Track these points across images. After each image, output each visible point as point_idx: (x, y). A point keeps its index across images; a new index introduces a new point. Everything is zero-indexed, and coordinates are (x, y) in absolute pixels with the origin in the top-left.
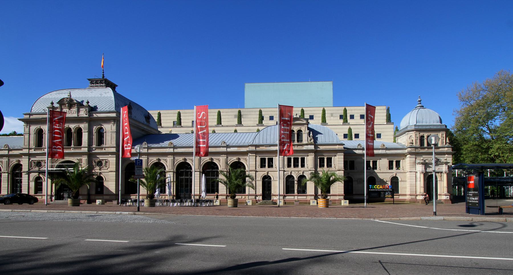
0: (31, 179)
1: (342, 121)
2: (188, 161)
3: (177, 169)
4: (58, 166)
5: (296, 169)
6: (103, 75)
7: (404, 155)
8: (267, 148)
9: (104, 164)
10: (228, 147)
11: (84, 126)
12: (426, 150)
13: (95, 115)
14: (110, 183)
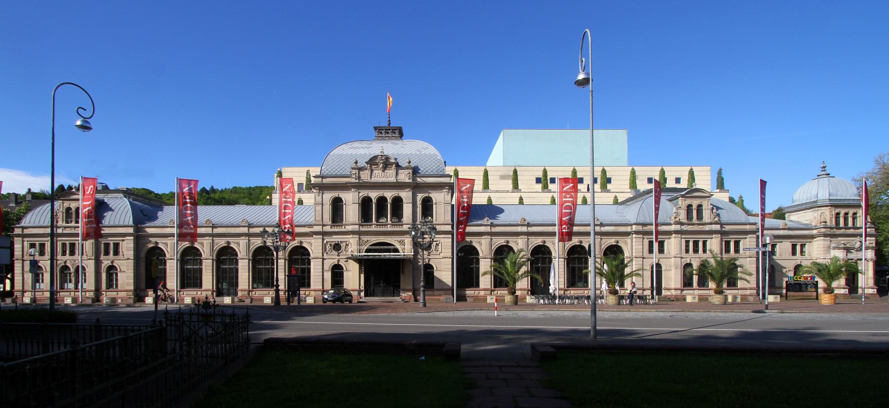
0: (327, 267)
1: (540, 186)
2: (304, 245)
3: (568, 254)
4: (368, 251)
5: (696, 255)
7: (813, 237)
9: (343, 248)
10: (528, 225)
12: (842, 231)
13: (419, 179)
14: (443, 273)
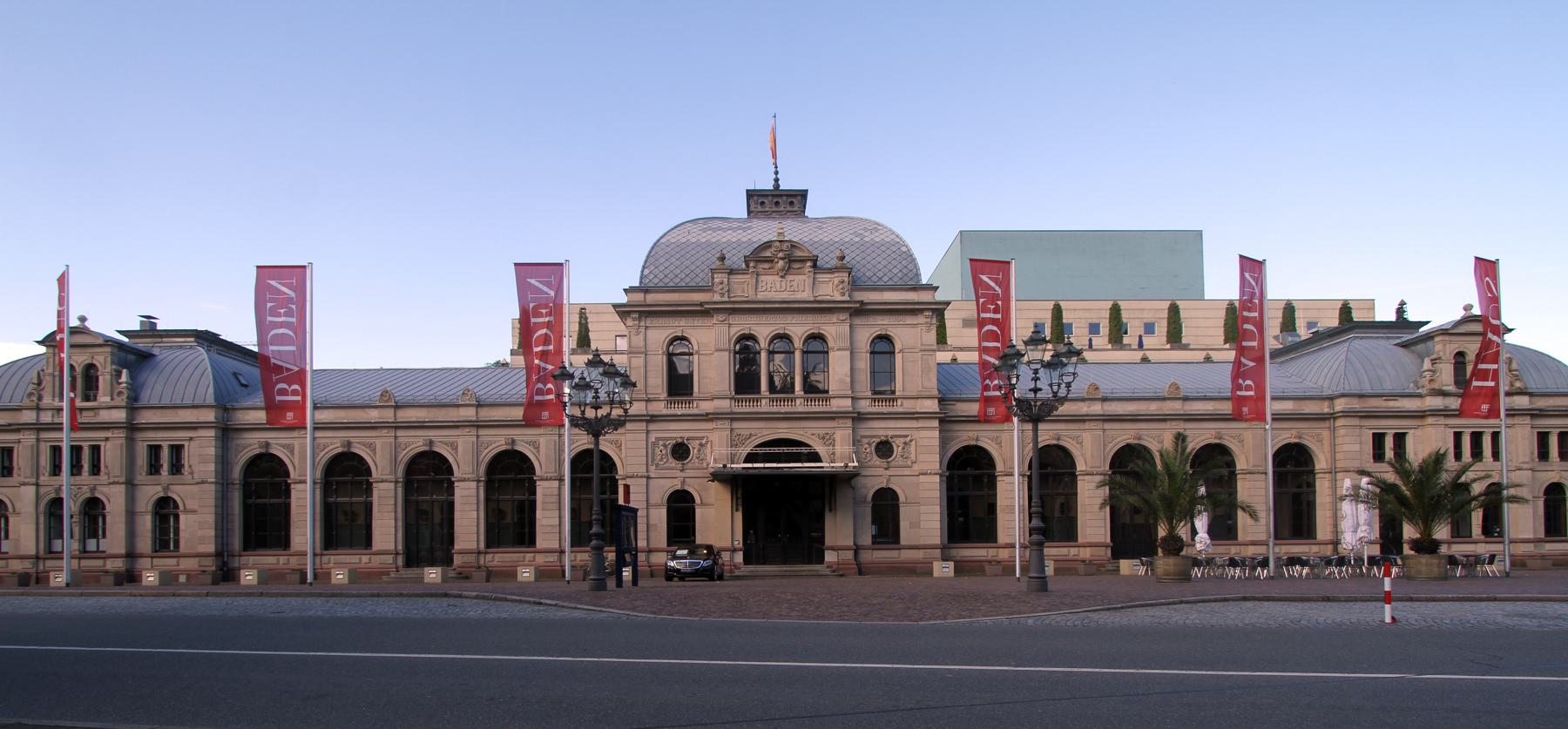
4: (750, 458)
6: (777, 180)
8: (1391, 404)
9: (694, 452)
10: (479, 405)
11: (834, 329)
